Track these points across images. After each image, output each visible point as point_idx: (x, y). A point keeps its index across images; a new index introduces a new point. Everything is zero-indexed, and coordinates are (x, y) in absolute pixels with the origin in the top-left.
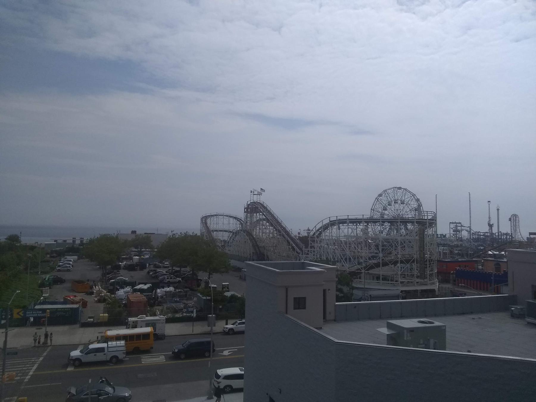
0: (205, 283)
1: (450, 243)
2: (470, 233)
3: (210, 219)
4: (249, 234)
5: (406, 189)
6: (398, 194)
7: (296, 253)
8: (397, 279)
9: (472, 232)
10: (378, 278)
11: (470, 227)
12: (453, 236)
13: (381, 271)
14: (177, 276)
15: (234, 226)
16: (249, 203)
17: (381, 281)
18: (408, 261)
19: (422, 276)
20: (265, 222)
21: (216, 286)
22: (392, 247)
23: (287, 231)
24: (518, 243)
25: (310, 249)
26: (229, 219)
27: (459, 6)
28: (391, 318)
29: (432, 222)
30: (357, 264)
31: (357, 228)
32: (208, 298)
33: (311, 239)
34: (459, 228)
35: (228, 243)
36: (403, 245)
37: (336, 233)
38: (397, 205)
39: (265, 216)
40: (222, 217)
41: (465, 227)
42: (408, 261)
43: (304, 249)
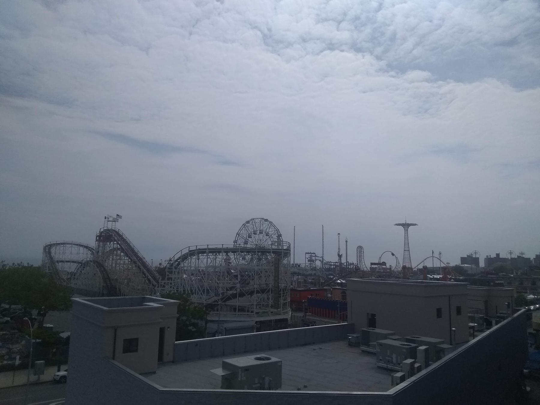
0: (38, 323)
1: (305, 272)
2: (323, 262)
3: (56, 248)
4: (100, 265)
5: (271, 222)
6: (264, 225)
7: (151, 286)
8: (252, 310)
9: (324, 261)
10: (235, 310)
11: (323, 257)
12: (308, 266)
13: (237, 302)
14: (4, 316)
15: (84, 255)
16: (102, 230)
17: (237, 313)
18: (263, 291)
19: (276, 306)
20: (120, 251)
21: (52, 326)
22: (250, 277)
23: (144, 262)
24: (361, 273)
25: (166, 281)
26: (79, 248)
27: (318, 54)
28: (235, 354)
29: (287, 253)
30: (214, 296)
31: (216, 258)
32: (38, 341)
33: (169, 270)
34: (314, 258)
35: (75, 276)
36: (260, 275)
37: (195, 263)
38: (261, 236)
39: (120, 245)
40: (71, 246)
41: (318, 257)
42: (263, 291)
43: (160, 281)
